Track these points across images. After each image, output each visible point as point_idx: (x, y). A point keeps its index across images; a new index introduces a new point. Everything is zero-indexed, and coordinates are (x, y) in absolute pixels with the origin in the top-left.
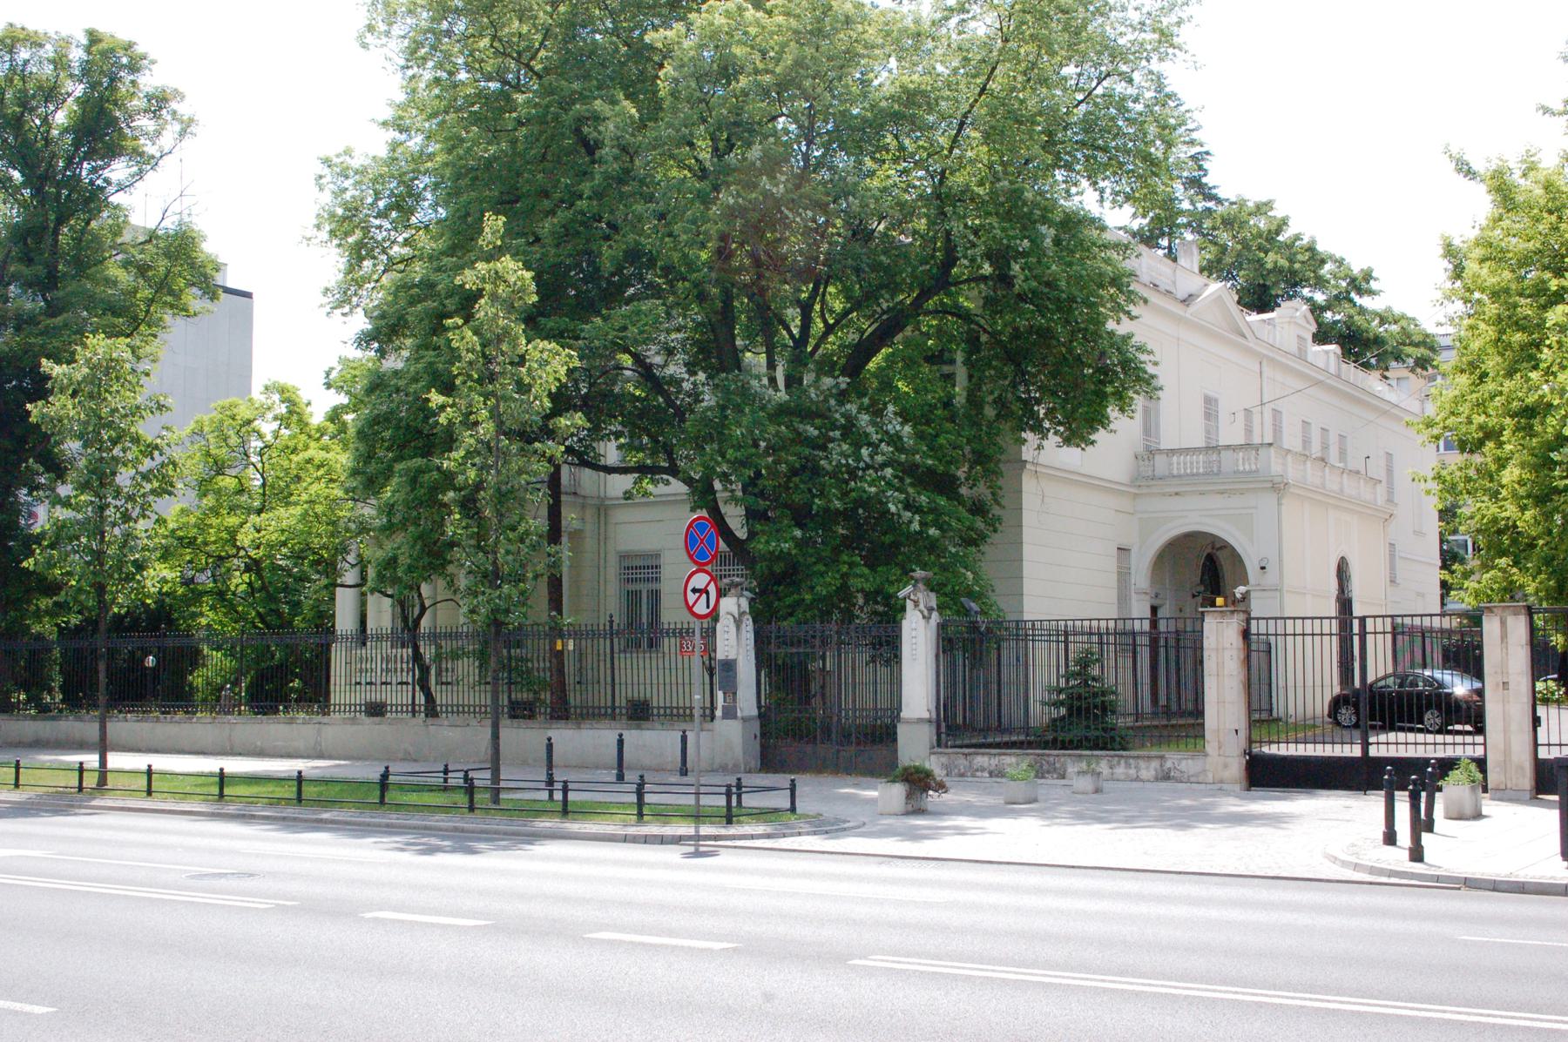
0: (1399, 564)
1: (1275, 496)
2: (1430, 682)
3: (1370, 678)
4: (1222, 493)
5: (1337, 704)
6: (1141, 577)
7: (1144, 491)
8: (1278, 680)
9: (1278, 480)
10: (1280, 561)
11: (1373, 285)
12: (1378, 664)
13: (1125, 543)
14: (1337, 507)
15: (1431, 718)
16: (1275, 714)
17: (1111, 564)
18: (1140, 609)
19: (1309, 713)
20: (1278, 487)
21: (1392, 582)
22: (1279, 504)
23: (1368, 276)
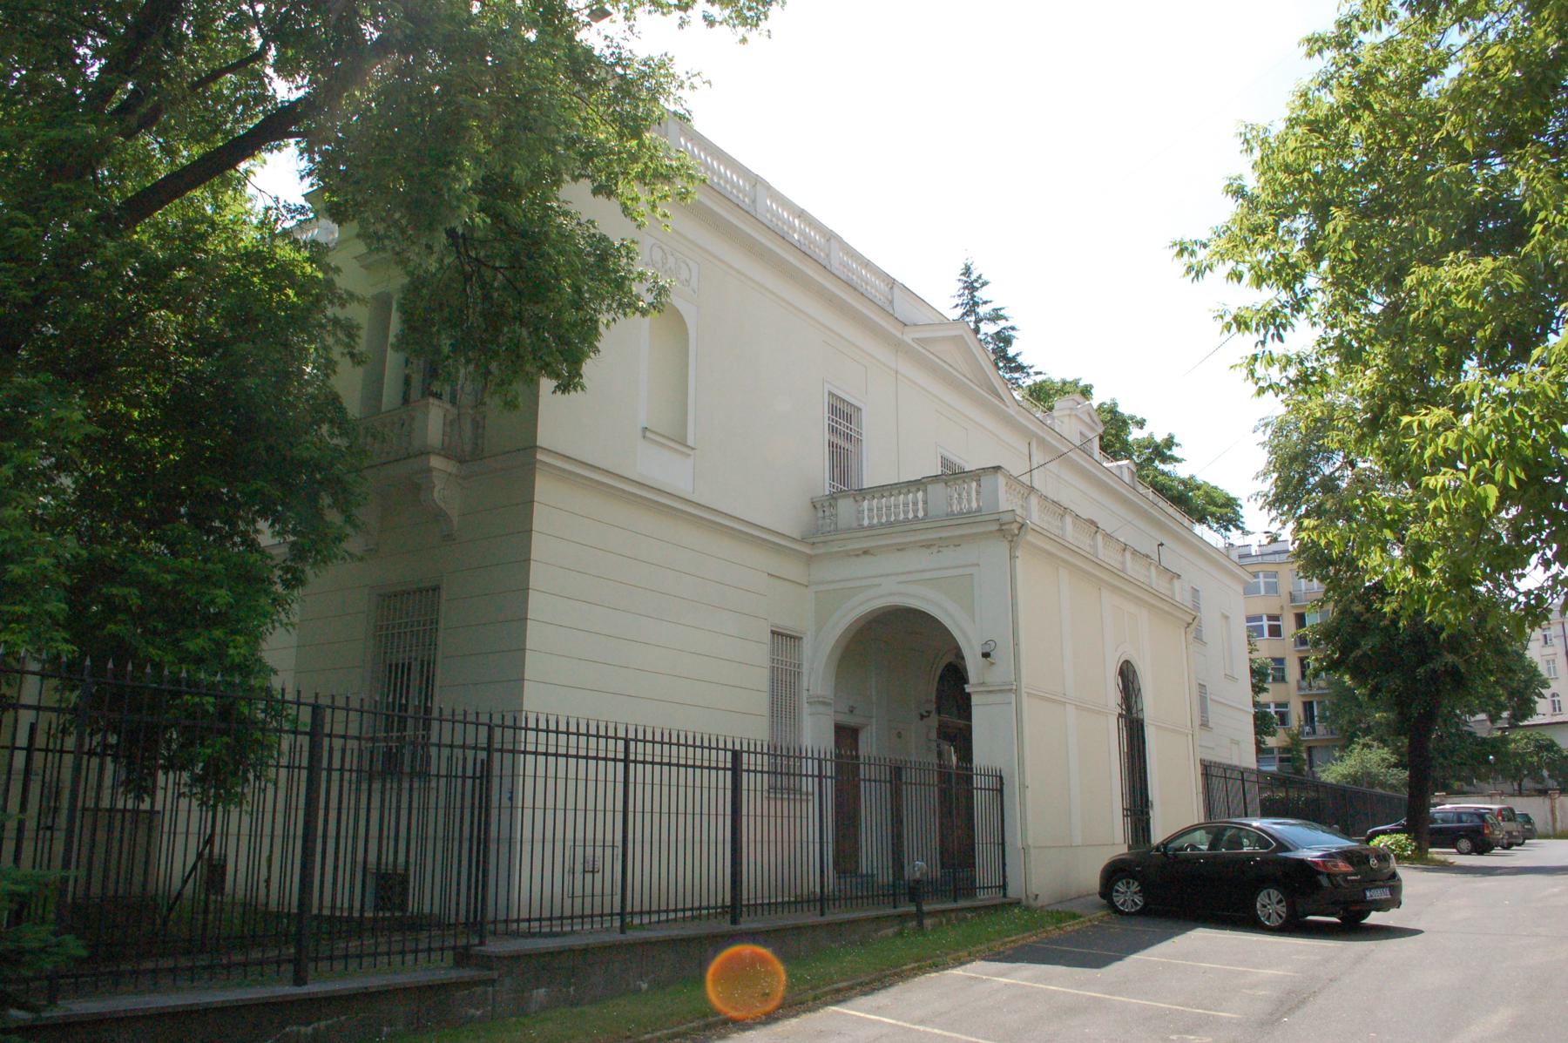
0: (1211, 707)
1: (1003, 547)
2: (1262, 839)
3: (1158, 835)
4: (928, 545)
5: (1115, 873)
6: (816, 674)
7: (821, 550)
8: (1014, 839)
9: (1006, 518)
10: (1016, 644)
11: (1175, 452)
12: (1177, 810)
13: (788, 623)
14: (1115, 589)
15: (1270, 904)
16: (412, 906)
17: (761, 653)
18: (815, 734)
19: (427, 910)
20: (1009, 531)
21: (1204, 724)
22: (1012, 557)
23: (1170, 442)
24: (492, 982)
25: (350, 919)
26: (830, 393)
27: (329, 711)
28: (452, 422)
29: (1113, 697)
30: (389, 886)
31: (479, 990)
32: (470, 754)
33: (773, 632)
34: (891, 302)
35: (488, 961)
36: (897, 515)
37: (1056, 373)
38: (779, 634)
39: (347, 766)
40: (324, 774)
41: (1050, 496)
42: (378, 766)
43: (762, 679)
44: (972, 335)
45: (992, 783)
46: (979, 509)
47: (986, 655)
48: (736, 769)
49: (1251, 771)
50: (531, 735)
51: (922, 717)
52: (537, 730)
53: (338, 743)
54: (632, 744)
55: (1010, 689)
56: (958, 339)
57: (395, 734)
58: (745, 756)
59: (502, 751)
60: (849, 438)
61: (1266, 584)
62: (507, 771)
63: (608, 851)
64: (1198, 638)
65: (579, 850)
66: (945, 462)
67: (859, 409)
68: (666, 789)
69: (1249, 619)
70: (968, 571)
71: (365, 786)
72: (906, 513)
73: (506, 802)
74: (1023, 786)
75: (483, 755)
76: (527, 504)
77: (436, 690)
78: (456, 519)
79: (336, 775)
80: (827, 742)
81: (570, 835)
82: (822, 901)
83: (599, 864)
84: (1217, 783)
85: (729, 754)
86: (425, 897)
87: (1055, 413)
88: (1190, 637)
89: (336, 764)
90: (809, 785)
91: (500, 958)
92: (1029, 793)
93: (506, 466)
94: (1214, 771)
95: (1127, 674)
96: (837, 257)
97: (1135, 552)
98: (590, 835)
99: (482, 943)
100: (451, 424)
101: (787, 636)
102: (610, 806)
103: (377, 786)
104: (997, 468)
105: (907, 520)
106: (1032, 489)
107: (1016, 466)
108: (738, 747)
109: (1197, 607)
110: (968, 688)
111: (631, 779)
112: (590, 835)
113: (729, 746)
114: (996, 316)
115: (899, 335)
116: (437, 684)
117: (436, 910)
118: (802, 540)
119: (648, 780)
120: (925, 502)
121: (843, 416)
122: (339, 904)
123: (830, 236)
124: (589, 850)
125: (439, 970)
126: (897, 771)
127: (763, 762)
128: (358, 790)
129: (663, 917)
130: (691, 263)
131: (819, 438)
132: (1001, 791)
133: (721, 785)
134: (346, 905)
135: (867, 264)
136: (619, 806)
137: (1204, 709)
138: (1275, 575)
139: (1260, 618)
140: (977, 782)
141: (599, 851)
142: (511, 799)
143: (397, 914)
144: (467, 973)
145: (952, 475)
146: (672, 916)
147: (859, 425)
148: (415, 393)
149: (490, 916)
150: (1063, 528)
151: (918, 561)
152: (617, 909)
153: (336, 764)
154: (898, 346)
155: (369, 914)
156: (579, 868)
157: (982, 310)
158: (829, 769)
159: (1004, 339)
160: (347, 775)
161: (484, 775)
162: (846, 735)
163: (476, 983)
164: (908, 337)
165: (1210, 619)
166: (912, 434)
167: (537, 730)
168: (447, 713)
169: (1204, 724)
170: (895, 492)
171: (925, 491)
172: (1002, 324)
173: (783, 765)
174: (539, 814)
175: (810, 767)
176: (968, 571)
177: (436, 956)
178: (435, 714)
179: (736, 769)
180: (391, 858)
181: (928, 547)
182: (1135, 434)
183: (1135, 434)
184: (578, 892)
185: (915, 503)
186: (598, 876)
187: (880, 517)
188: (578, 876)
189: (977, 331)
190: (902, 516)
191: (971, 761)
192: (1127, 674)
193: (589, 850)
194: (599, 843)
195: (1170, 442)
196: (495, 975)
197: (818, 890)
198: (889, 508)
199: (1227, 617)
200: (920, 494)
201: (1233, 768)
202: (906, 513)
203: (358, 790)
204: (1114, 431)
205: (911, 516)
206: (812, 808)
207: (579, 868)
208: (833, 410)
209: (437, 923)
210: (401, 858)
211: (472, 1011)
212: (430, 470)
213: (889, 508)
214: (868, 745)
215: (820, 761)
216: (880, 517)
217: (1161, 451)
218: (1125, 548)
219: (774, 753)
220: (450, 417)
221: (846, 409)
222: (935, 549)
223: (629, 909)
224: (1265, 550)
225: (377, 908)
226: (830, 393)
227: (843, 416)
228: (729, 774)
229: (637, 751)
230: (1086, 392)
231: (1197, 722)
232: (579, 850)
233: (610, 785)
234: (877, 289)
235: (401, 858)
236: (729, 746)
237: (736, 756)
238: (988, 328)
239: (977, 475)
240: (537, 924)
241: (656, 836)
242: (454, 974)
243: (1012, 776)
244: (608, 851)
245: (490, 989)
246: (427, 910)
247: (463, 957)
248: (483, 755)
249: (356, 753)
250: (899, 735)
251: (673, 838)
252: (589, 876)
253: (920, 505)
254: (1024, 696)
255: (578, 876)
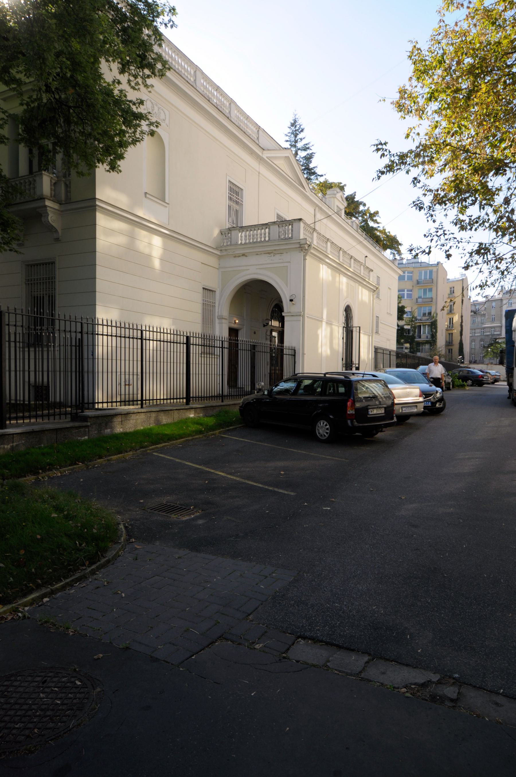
0: (380, 325)
6: (223, 306)
7: (225, 253)
9: (303, 242)
10: (304, 296)
16: (52, 399)
17: (198, 297)
18: (221, 331)
19: (58, 400)
22: (305, 259)
24: (87, 426)
25: (24, 404)
26: (229, 181)
27: (7, 314)
28: (55, 184)
29: (342, 319)
30: (41, 391)
31: (82, 430)
32: (73, 335)
33: (204, 288)
34: (258, 138)
35: (85, 419)
36: (257, 239)
37: (332, 179)
38: (206, 289)
39: (18, 340)
40: (7, 343)
41: (322, 233)
42: (32, 341)
43: (198, 308)
44: (293, 157)
45: (292, 352)
46: (291, 238)
47: (291, 300)
48: (188, 344)
49: (393, 351)
50: (100, 327)
51: (264, 326)
52: (103, 325)
53: (12, 329)
54: (144, 332)
55: (300, 315)
56: (287, 158)
57: (39, 328)
58: (192, 338)
59: (146, 339)
60: (237, 203)
61: (408, 276)
62: (90, 343)
63: (135, 377)
64: (378, 297)
65: (123, 376)
66: (278, 216)
67: (242, 190)
68: (169, 353)
69: (399, 291)
70: (285, 264)
71: (26, 349)
72: (261, 238)
73: (90, 356)
74: (303, 354)
75: (79, 336)
76: (93, 225)
77: (57, 308)
78: (60, 231)
79: (13, 344)
80: (226, 334)
81: (118, 370)
82: (222, 397)
83: (131, 382)
84: (380, 356)
85: (185, 338)
86: (57, 394)
87: (327, 196)
88: (375, 296)
89: (12, 339)
90: (218, 351)
91: (91, 418)
92: (305, 356)
93: (83, 207)
94: (379, 351)
95: (348, 310)
96: (235, 113)
97: (355, 260)
98: (127, 370)
99: (83, 412)
100: (55, 185)
101: (209, 290)
102: (135, 359)
103: (32, 349)
104: (300, 220)
105: (261, 242)
106: (314, 229)
107: (309, 220)
108: (188, 335)
109: (378, 284)
110: (283, 314)
111: (144, 348)
112: (127, 370)
113: (185, 334)
114: (305, 148)
115: (260, 154)
116: (57, 305)
117: (62, 400)
118: (216, 249)
119: (127, 346)
120: (269, 234)
121: (235, 193)
122: (18, 398)
123: (232, 102)
124: (127, 377)
125: (65, 423)
126: (254, 347)
127: (199, 341)
128: (24, 352)
129: (162, 402)
130: (164, 110)
131: (224, 202)
132: (295, 355)
133: (135, 347)
134: (22, 399)
135: (248, 117)
136: (139, 359)
137: (377, 326)
138: (412, 272)
139: (404, 291)
140: (285, 351)
141: (131, 377)
142: (93, 355)
143: (45, 402)
144: (77, 424)
145: (282, 222)
146: (162, 402)
147: (242, 197)
148: (35, 168)
149: (86, 401)
150: (326, 248)
151: (264, 259)
152: (139, 398)
153: (12, 339)
154: (260, 159)
155: (32, 402)
156: (123, 384)
157: (300, 145)
158: (226, 345)
159: (309, 158)
160: (18, 344)
161: (80, 344)
162: (233, 332)
163: (83, 427)
164: (265, 155)
165: (383, 289)
166: (269, 200)
167: (103, 325)
168: (62, 317)
169: (377, 332)
170: (256, 229)
171: (269, 229)
172: (309, 152)
173: (208, 343)
174: (123, 362)
175: (218, 344)
176: (285, 264)
177: (63, 417)
178: (57, 317)
179: (188, 344)
180: (41, 380)
181: (269, 253)
182: (361, 208)
183: (361, 208)
184: (123, 393)
185: (265, 234)
186: (131, 387)
187: (249, 240)
188: (123, 387)
189: (296, 154)
190: (259, 240)
191: (283, 343)
192: (348, 310)
193: (127, 377)
194: (131, 373)
195: (377, 213)
196: (89, 424)
197: (221, 393)
198: (253, 236)
199: (390, 289)
200: (267, 230)
201: (386, 350)
202: (261, 238)
203: (24, 352)
204: (353, 207)
205: (263, 239)
206: (219, 361)
207: (123, 384)
208: (231, 189)
209: (60, 405)
210: (45, 380)
211: (79, 438)
212: (46, 206)
213: (253, 236)
214: (242, 337)
215: (222, 342)
216: (249, 240)
217: (373, 216)
218: (351, 257)
219: (204, 337)
220: (53, 181)
221: (237, 190)
222: (272, 255)
223: (144, 399)
224: (409, 261)
225: (36, 400)
226: (229, 181)
227: (235, 193)
228: (185, 345)
229: (146, 335)
230: (342, 188)
231: (374, 331)
232: (123, 376)
233: (182, 354)
234: (251, 130)
235: (45, 380)
236: (185, 334)
237: (188, 338)
238: (302, 154)
239: (291, 222)
240: (110, 404)
241: (165, 372)
242: (71, 424)
243: (299, 349)
244: (135, 377)
245: (87, 429)
246: (58, 400)
247: (75, 418)
248: (79, 336)
249: (21, 335)
250: (255, 333)
251: (165, 372)
252: (127, 387)
253: (267, 234)
254: (306, 318)
255: (123, 387)
